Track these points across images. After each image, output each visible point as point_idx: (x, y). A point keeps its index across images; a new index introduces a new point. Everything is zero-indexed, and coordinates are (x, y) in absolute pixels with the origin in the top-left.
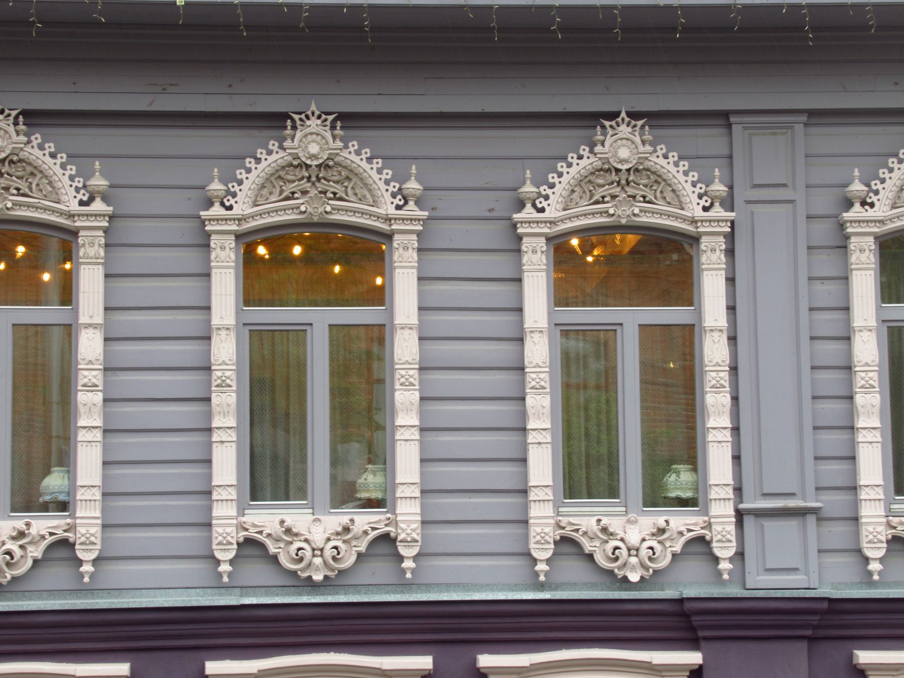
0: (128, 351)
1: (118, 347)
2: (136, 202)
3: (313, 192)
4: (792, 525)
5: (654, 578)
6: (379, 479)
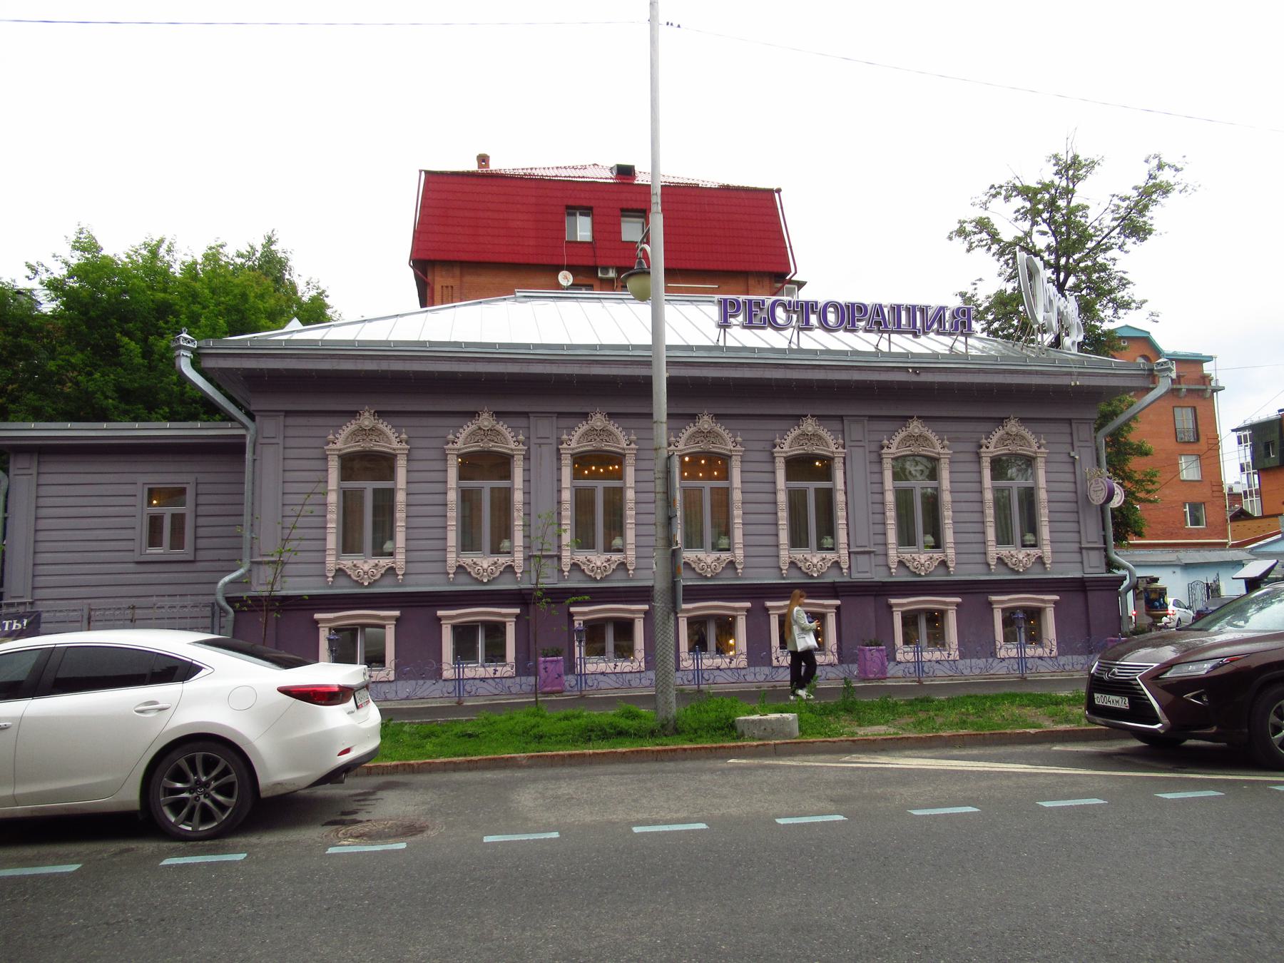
2: (417, 443)
4: (866, 557)
5: (821, 575)
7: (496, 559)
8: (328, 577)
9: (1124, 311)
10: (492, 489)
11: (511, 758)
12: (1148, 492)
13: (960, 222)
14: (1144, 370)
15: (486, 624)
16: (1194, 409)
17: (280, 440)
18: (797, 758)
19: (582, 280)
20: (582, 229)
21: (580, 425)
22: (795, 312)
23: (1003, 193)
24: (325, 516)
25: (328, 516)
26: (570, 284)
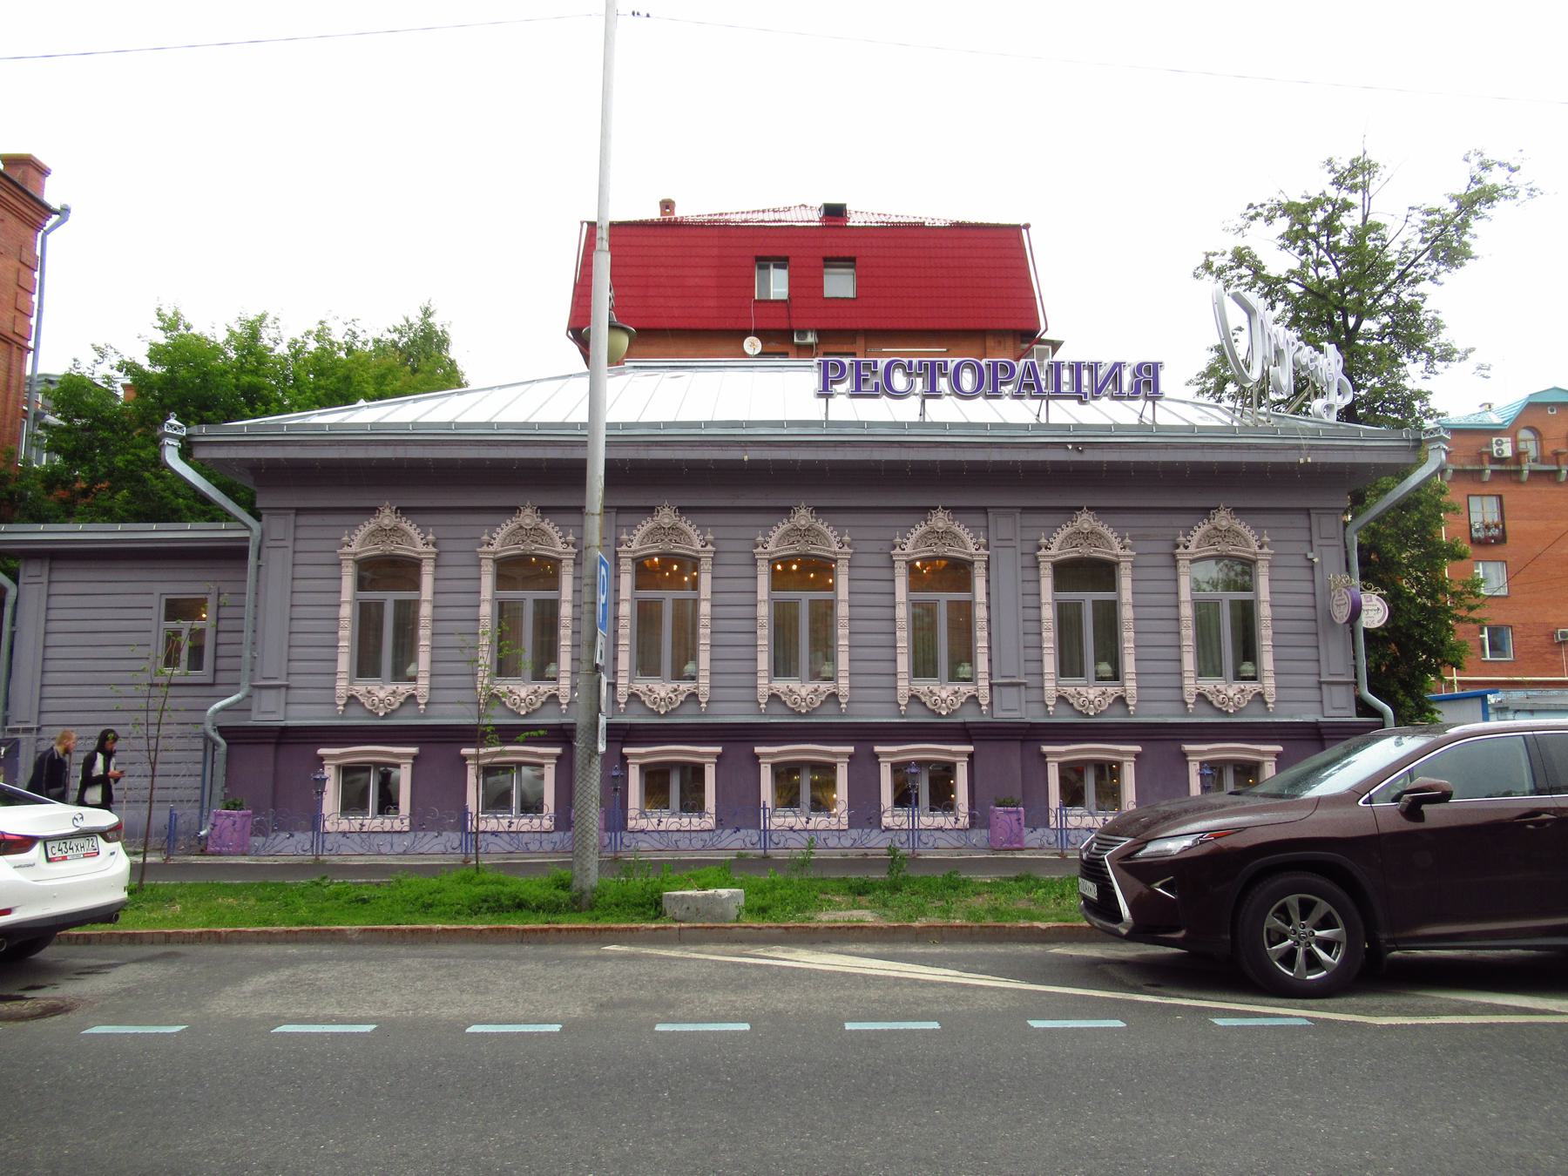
0: (721, 611)
1: (718, 609)
2: (725, 545)
3: (802, 541)
4: (1014, 690)
6: (830, 669)
7: (536, 687)
8: (338, 705)
9: (1444, 364)
10: (1095, 602)
11: (339, 930)
12: (1471, 608)
13: (1208, 255)
14: (1409, 440)
15: (683, 766)
16: (1500, 497)
17: (289, 543)
18: (705, 947)
19: (774, 347)
20: (777, 284)
21: (644, 522)
22: (919, 375)
23: (1266, 213)
24: (337, 633)
25: (340, 633)
26: (757, 352)
